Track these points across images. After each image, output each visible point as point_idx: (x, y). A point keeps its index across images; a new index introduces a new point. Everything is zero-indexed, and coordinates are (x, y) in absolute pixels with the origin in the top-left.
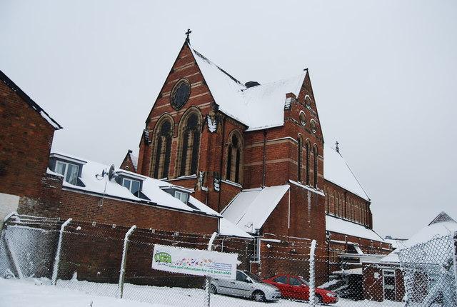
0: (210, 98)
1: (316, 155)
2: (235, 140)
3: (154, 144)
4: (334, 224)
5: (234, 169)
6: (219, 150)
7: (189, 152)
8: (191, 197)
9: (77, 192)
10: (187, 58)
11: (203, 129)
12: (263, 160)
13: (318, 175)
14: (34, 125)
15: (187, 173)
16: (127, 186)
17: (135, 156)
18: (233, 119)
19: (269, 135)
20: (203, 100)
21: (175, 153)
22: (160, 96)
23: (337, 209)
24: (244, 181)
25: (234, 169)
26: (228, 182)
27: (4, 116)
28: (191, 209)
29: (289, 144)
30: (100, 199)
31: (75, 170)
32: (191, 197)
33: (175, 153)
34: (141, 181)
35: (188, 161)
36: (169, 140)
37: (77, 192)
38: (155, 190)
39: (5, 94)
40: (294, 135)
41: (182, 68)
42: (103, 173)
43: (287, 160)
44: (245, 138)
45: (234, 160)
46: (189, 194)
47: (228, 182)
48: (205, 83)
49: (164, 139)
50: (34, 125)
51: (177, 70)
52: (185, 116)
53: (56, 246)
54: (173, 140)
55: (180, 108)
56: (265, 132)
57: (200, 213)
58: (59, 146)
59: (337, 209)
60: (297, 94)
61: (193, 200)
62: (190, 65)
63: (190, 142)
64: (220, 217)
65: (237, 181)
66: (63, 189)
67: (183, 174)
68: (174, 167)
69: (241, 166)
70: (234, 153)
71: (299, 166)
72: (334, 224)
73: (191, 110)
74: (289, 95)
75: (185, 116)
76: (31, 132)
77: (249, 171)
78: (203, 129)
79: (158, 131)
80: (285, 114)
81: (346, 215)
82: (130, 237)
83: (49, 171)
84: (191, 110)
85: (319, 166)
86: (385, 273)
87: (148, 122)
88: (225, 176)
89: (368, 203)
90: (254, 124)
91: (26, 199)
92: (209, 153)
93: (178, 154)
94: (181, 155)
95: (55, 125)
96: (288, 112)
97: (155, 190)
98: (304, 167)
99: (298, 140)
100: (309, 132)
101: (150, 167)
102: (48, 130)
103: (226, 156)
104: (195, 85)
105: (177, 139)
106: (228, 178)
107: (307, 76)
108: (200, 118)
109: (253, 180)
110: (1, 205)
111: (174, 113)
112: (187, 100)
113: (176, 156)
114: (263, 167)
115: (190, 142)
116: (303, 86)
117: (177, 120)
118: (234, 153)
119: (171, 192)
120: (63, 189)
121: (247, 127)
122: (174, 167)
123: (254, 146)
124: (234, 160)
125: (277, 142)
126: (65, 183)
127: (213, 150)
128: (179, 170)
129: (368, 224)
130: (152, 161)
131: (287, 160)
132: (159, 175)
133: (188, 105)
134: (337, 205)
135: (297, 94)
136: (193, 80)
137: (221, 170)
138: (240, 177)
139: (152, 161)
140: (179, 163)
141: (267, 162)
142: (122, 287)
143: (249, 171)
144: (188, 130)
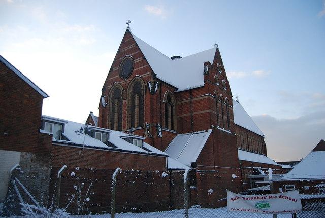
0: (149, 69)
1: (228, 106)
2: (169, 99)
3: (109, 106)
4: (243, 155)
5: (170, 120)
6: (159, 107)
7: (136, 110)
8: (144, 143)
9: (63, 145)
10: (129, 41)
11: (146, 93)
12: (191, 112)
13: (230, 120)
14: (28, 96)
15: (136, 125)
16: (98, 138)
17: (96, 113)
18: (166, 83)
19: (194, 93)
20: (144, 71)
21: (126, 112)
22: (111, 71)
23: (242, 144)
24: (178, 129)
25: (170, 120)
26: (167, 130)
27: (4, 90)
28: (147, 152)
29: (209, 99)
30: (81, 149)
31: (58, 128)
32: (144, 143)
33: (126, 112)
34: (108, 133)
35: (136, 117)
36: (120, 102)
37: (63, 145)
38: (117, 138)
39: (4, 73)
40: (212, 93)
41: (126, 49)
42: (82, 129)
43: (209, 110)
44: (176, 97)
45: (169, 114)
46: (143, 141)
47: (167, 130)
48: (144, 58)
49: (116, 102)
50: (28, 96)
51: (123, 50)
52: (131, 83)
53: (263, 183)
54: (124, 102)
55: (127, 78)
56: (191, 92)
57: (153, 154)
58: (49, 109)
59: (242, 144)
60: (212, 62)
61: (146, 145)
62: (132, 46)
63: (136, 102)
64: (167, 156)
65: (172, 129)
66: (53, 144)
67: (134, 127)
68: (125, 122)
69: (174, 117)
70: (169, 109)
71: (218, 115)
72: (243, 155)
73: (136, 79)
74: (206, 64)
75: (131, 83)
76: (25, 102)
77: (181, 121)
78: (146, 93)
79: (112, 96)
80: (205, 77)
81: (249, 149)
82: (117, 177)
83: (41, 131)
84: (136, 79)
85: (230, 114)
86: (287, 187)
87: (103, 90)
88: (164, 125)
89: (262, 138)
90: (182, 86)
91: (26, 154)
92: (152, 110)
93: (128, 112)
94: (130, 112)
95: (44, 95)
96: (206, 75)
97: (117, 138)
98: (220, 115)
99: (215, 96)
100: (222, 90)
101: (108, 122)
102: (36, 97)
103: (164, 111)
104: (137, 61)
105: (126, 101)
106: (167, 127)
107: (217, 49)
108: (143, 84)
109: (188, 127)
110: (13, 159)
111: (123, 82)
112: (132, 72)
113: (127, 113)
114: (191, 117)
115: (136, 102)
116: (215, 56)
117: (126, 87)
118: (169, 109)
119: (129, 140)
120: (53, 144)
121: (177, 89)
122: (125, 122)
123: (183, 102)
124: (169, 114)
125: (200, 98)
126: (54, 140)
127: (155, 107)
128: (130, 124)
129: (263, 151)
130: (108, 118)
131: (209, 110)
132: (115, 128)
133: (132, 76)
134: (242, 141)
135: (212, 62)
136: (135, 57)
137: (161, 120)
138: (174, 125)
139: (108, 118)
140: (130, 118)
141: (194, 113)
142: (187, 213)
143: (181, 121)
144: (134, 93)
